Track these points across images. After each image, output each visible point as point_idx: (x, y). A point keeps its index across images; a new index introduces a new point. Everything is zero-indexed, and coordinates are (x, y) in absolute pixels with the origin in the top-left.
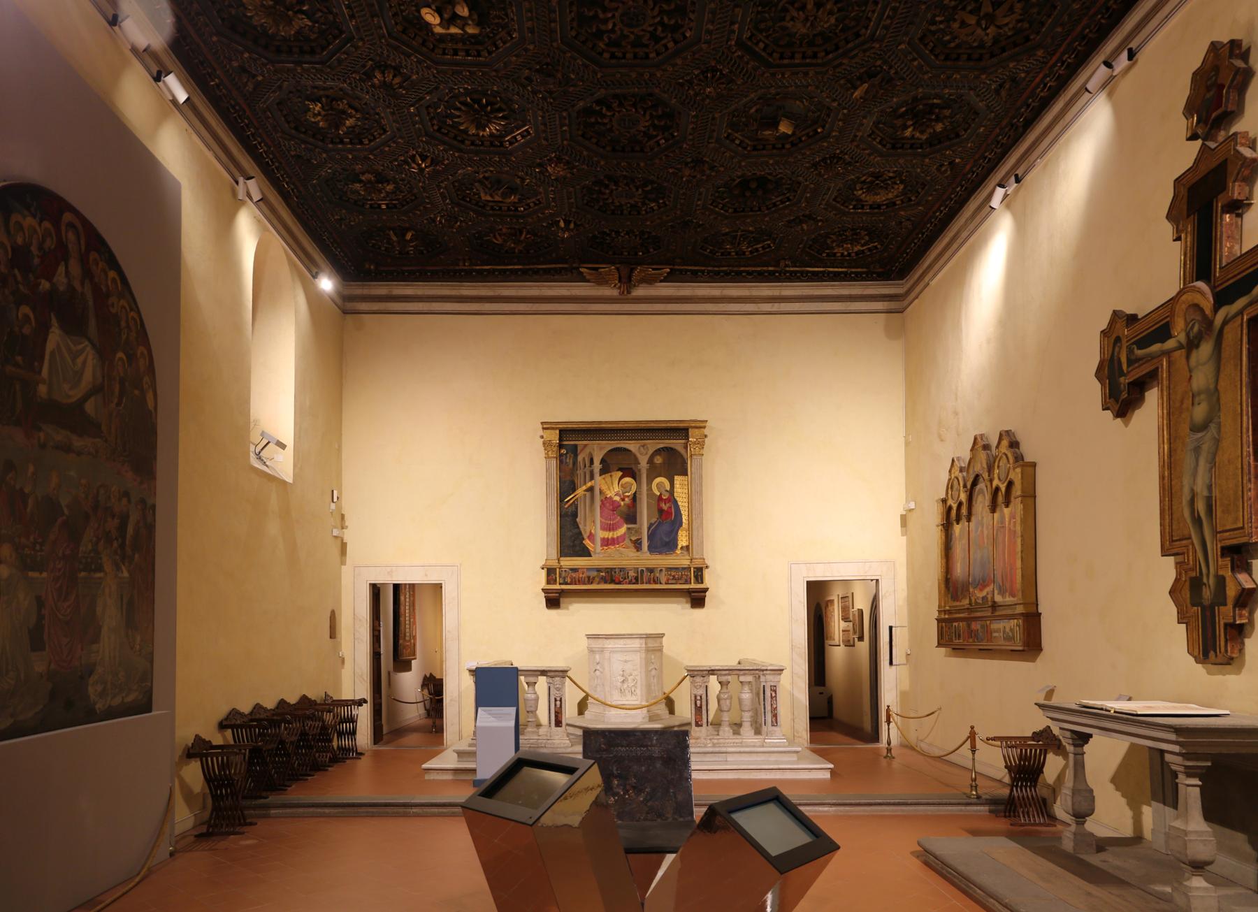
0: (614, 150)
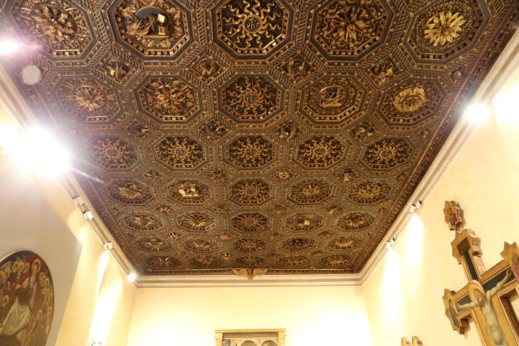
0: (245, 230)
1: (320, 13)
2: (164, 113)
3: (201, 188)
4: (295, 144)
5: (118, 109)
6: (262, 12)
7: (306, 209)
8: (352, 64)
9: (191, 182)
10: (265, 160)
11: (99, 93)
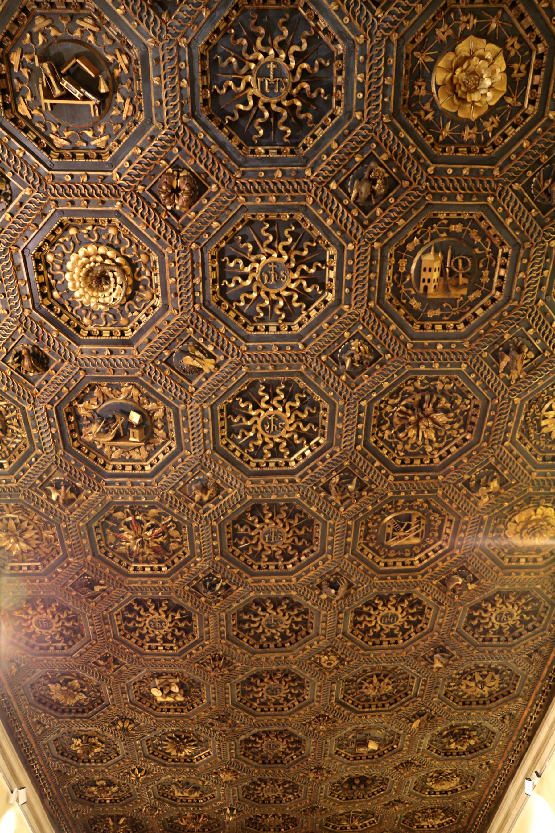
0: (264, 763)
1: (376, 404)
2: (132, 560)
3: (188, 686)
4: (347, 608)
5: (58, 553)
6: (287, 406)
7: (370, 720)
8: (432, 478)
9: (172, 674)
10: (297, 636)
11: (31, 527)
